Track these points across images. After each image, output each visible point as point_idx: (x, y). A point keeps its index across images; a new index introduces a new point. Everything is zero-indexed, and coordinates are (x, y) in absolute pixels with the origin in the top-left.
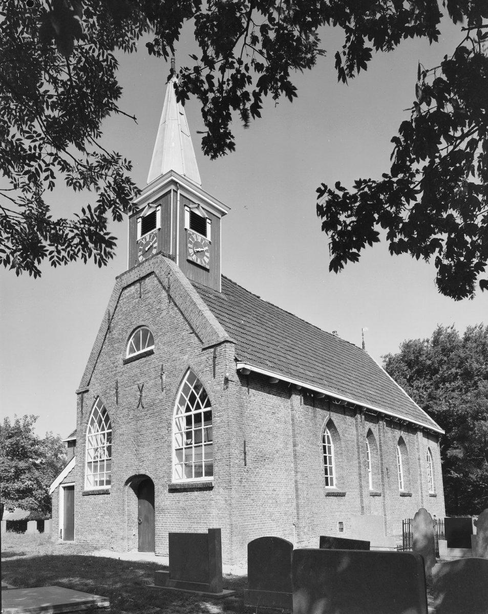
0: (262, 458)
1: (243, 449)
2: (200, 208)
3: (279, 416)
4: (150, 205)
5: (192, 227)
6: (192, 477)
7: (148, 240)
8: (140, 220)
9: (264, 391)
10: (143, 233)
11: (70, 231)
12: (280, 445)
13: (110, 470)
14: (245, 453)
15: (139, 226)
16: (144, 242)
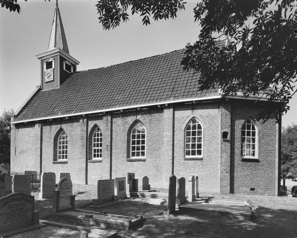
0: (22, 152)
1: (15, 150)
2: (50, 58)
3: (31, 135)
4: (50, 58)
5: (66, 69)
6: (95, 147)
7: (49, 72)
8: (45, 63)
9: (25, 128)
10: (47, 68)
11: (220, 94)
12: (30, 146)
13: (101, 147)
14: (16, 151)
15: (45, 66)
16: (47, 72)
